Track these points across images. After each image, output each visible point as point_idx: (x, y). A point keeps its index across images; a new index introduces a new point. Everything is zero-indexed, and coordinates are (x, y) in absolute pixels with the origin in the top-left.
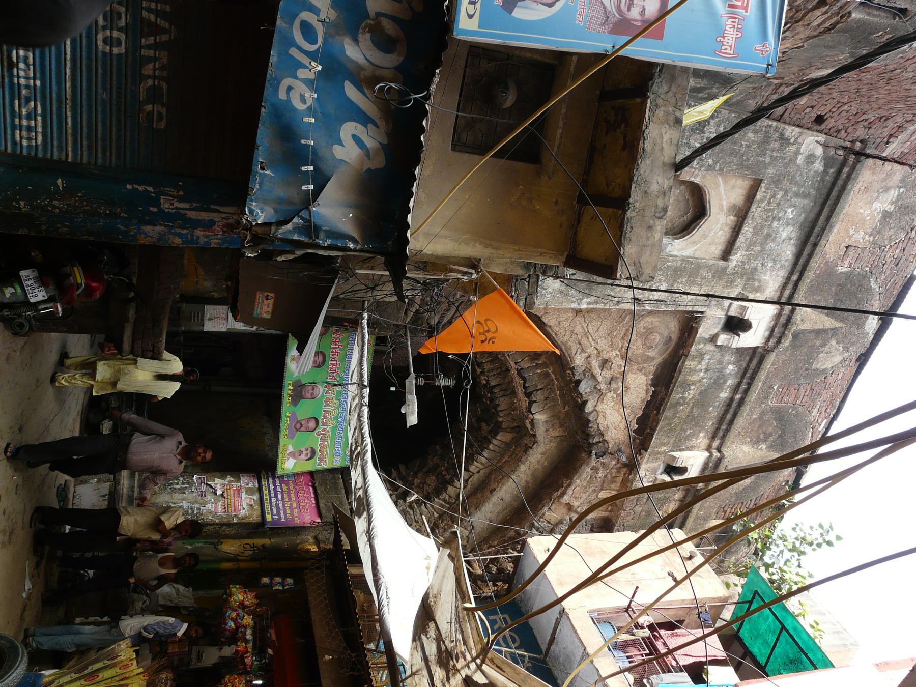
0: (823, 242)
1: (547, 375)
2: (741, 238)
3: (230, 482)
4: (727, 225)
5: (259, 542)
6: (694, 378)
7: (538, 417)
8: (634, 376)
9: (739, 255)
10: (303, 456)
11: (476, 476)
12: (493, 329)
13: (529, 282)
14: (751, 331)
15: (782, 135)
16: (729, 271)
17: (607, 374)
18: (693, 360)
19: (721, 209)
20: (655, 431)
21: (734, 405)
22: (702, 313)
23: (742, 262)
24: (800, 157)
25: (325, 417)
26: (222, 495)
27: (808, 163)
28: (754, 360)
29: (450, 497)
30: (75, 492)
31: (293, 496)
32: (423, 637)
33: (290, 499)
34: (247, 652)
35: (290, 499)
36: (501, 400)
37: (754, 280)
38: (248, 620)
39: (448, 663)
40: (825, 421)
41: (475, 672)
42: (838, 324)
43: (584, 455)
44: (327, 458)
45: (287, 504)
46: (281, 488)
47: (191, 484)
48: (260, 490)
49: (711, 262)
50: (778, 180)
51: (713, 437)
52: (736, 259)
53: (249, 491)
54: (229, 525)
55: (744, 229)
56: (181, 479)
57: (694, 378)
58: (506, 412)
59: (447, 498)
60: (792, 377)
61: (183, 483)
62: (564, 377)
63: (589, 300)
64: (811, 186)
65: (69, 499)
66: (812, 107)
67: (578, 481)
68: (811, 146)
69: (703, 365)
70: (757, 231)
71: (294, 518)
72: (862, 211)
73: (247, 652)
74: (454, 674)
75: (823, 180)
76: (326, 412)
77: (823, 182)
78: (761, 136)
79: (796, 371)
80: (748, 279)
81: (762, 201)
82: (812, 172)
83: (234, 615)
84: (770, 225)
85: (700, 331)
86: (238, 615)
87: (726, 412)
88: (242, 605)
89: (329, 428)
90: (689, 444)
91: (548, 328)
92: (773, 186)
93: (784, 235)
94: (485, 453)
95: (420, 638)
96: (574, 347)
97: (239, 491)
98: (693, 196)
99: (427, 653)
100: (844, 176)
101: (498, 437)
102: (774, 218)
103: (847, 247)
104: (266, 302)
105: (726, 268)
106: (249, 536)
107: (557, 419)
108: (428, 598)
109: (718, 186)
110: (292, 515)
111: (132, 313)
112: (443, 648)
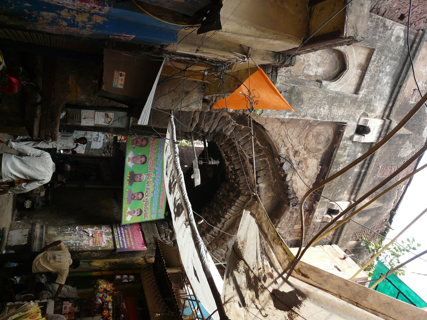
0: (404, 85)
1: (265, 161)
2: (365, 82)
3: (96, 229)
4: (357, 75)
5: (113, 260)
6: (342, 160)
7: (261, 185)
8: (311, 160)
9: (363, 91)
10: (136, 214)
11: (229, 220)
12: (257, 96)
13: (272, 76)
14: (370, 133)
15: (384, 24)
16: (359, 100)
17: (297, 159)
18: (341, 150)
19: (354, 66)
20: (322, 190)
21: (362, 175)
22: (345, 123)
23: (365, 95)
24: (393, 37)
25: (147, 192)
26: (92, 236)
27: (396, 41)
28: (372, 149)
29: (215, 233)
30: (8, 234)
31: (131, 236)
32: (235, 273)
33: (129, 237)
34: (109, 316)
35: (129, 237)
36: (241, 177)
37: (371, 106)
38: (109, 298)
39: (257, 285)
40: (404, 186)
41: (282, 284)
42: (410, 133)
43: (285, 205)
44: (149, 215)
45: (128, 240)
46: (124, 232)
47: (75, 231)
48: (113, 233)
49: (350, 95)
50: (382, 50)
51: (351, 194)
52: (362, 93)
53: (107, 234)
54: (96, 251)
55: (366, 77)
56: (69, 229)
57: (342, 160)
58: (244, 184)
59: (214, 233)
60: (388, 161)
61: (70, 231)
62: (274, 163)
63: (289, 113)
64: (398, 54)
65: (5, 237)
66: (399, 9)
67: (283, 220)
68: (398, 32)
69: (346, 153)
70: (372, 78)
71: (132, 246)
72: (421, 70)
73: (109, 316)
74: (262, 292)
75: (404, 51)
76: (147, 189)
77: (404, 52)
78: (374, 24)
79: (390, 158)
80: (368, 105)
81: (374, 61)
82: (399, 46)
83: (101, 295)
84: (378, 75)
85: (345, 133)
86: (103, 295)
87: (357, 179)
88: (105, 290)
89: (149, 198)
90: (340, 197)
91: (267, 132)
92: (380, 53)
93: (385, 81)
94: (233, 208)
95: (232, 274)
96: (281, 143)
97: (101, 234)
98: (339, 59)
99: (239, 283)
100: (414, 49)
101: (240, 199)
102: (380, 71)
103: (414, 90)
104: (120, 78)
105: (357, 98)
106: (107, 257)
107: (271, 187)
108: (237, 245)
109: (352, 53)
110: (131, 244)
111: (38, 112)
112: (252, 275)
